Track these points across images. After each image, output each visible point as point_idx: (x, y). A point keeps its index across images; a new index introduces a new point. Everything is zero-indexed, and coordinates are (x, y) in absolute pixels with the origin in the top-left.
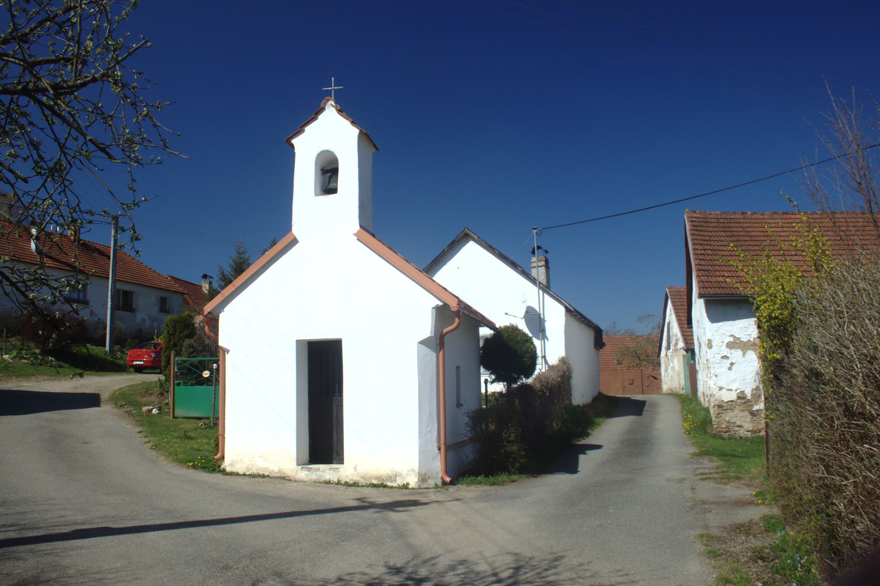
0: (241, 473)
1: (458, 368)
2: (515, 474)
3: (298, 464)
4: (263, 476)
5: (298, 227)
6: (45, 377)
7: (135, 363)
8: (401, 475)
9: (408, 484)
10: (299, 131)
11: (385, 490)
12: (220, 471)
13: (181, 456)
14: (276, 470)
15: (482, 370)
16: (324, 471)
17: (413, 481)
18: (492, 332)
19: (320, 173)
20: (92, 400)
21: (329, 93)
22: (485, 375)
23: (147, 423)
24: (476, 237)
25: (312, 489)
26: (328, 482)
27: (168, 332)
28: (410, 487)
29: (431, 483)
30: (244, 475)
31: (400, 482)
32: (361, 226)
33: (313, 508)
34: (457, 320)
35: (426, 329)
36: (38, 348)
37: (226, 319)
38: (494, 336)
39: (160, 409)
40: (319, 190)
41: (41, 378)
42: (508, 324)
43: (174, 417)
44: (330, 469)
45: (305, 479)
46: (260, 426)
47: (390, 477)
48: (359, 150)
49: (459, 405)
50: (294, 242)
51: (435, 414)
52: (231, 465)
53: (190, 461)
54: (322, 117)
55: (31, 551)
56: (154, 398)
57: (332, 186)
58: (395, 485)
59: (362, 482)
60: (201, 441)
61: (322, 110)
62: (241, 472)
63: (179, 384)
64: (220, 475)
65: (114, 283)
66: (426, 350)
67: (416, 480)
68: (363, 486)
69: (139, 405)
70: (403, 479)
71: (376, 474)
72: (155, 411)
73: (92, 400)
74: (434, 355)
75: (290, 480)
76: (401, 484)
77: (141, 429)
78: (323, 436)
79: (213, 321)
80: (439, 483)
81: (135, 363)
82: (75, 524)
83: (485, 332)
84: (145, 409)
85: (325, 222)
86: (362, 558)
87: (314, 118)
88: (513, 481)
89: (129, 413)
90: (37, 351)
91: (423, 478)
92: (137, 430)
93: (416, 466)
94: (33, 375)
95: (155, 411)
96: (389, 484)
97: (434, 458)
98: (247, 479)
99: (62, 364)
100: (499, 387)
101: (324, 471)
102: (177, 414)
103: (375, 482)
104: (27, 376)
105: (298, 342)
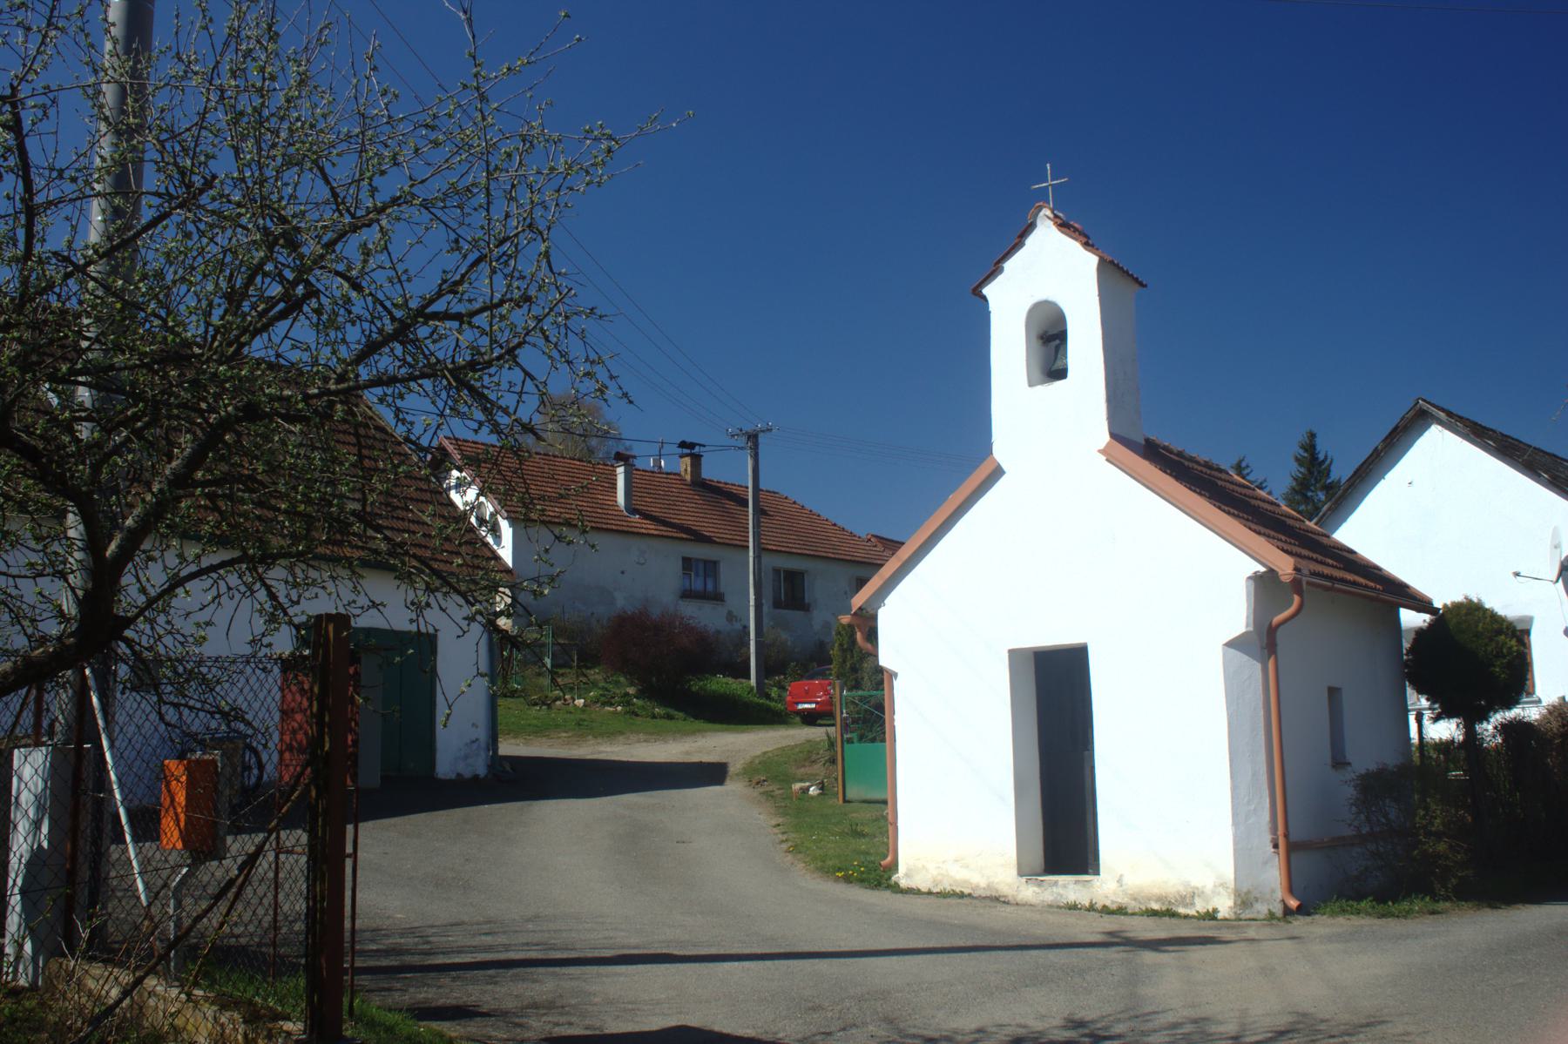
0: (924, 889)
1: (1333, 692)
2: (1447, 899)
3: (1021, 874)
4: (962, 895)
5: (1004, 445)
6: (641, 736)
7: (800, 707)
8: (1202, 894)
9: (1215, 911)
10: (995, 271)
11: (1174, 921)
12: (889, 887)
13: (830, 863)
14: (983, 884)
15: (1410, 693)
16: (1065, 886)
17: (1224, 905)
18: (1427, 617)
19: (1037, 344)
20: (713, 774)
21: (1042, 196)
22: (1419, 702)
23: (795, 812)
24: (1442, 415)
25: (1037, 916)
26: (1073, 907)
27: (841, 645)
28: (1220, 916)
29: (1261, 909)
30: (930, 893)
31: (1200, 906)
32: (1112, 435)
33: (1015, 941)
34: (1296, 599)
35: (1236, 617)
36: (632, 684)
37: (890, 618)
38: (1431, 626)
39: (822, 787)
40: (1037, 374)
41: (633, 737)
42: (1459, 598)
43: (845, 801)
44: (1076, 882)
45: (1034, 900)
46: (954, 811)
47: (1183, 898)
48: (1101, 295)
49: (1339, 762)
50: (998, 472)
51: (1264, 778)
52: (907, 875)
53: (840, 870)
54: (1030, 241)
55: (554, 974)
56: (819, 769)
57: (1058, 365)
58: (1192, 912)
59: (1133, 906)
60: (850, 831)
61: (1030, 228)
62: (924, 888)
63: (850, 741)
64: (887, 894)
65: (757, 558)
66: (1239, 657)
67: (1230, 903)
68: (1133, 914)
69: (788, 780)
70: (1207, 902)
71: (1156, 891)
72: (813, 791)
73: (713, 774)
74: (1258, 666)
75: (1007, 903)
76: (1202, 910)
77: (780, 820)
78: (1063, 823)
79: (868, 624)
80: (1278, 910)
81: (800, 707)
82: (629, 947)
83: (1411, 619)
84: (797, 786)
85: (1050, 431)
86: (1044, 1008)
87: (1018, 244)
88: (1433, 913)
89: (769, 795)
90: (631, 690)
91: (1244, 900)
92: (774, 822)
93: (1229, 873)
94: (621, 733)
95: (813, 791)
96: (1182, 910)
97: (1265, 863)
98: (932, 899)
99: (672, 712)
100: (1445, 730)
101: (1065, 886)
102: (850, 794)
103: (1156, 906)
104: (611, 735)
105: (1013, 654)
